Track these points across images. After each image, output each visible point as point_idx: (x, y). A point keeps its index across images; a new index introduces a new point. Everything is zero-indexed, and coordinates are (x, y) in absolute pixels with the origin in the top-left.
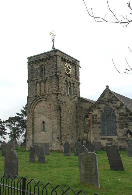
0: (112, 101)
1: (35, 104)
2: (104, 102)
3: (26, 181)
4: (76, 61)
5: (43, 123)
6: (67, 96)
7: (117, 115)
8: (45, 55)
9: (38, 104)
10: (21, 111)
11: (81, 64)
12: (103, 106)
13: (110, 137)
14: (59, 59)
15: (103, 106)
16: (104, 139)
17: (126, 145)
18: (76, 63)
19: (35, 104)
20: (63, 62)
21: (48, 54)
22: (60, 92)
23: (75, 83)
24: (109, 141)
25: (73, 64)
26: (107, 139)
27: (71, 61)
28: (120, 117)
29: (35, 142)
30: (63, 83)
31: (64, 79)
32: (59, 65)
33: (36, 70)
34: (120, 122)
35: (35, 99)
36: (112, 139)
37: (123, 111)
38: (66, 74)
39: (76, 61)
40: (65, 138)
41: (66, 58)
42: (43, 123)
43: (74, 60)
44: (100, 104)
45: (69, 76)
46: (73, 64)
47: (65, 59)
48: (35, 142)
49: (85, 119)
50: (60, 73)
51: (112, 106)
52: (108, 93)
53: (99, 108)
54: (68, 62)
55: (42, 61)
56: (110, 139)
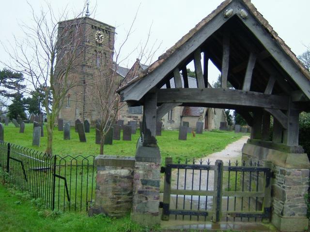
3: (54, 43)
4: (111, 28)
11: (116, 31)
13: (136, 115)
14: (88, 27)
16: (130, 117)
20: (94, 30)
23: (107, 53)
24: (134, 119)
25: (106, 31)
26: (133, 117)
27: (104, 28)
29: (108, 203)
32: (87, 34)
36: (137, 117)
38: (96, 42)
39: (111, 28)
40: (88, 115)
41: (98, 25)
43: (108, 27)
45: (100, 45)
46: (106, 31)
47: (96, 27)
48: (108, 203)
50: (89, 42)
54: (99, 29)
56: (136, 117)
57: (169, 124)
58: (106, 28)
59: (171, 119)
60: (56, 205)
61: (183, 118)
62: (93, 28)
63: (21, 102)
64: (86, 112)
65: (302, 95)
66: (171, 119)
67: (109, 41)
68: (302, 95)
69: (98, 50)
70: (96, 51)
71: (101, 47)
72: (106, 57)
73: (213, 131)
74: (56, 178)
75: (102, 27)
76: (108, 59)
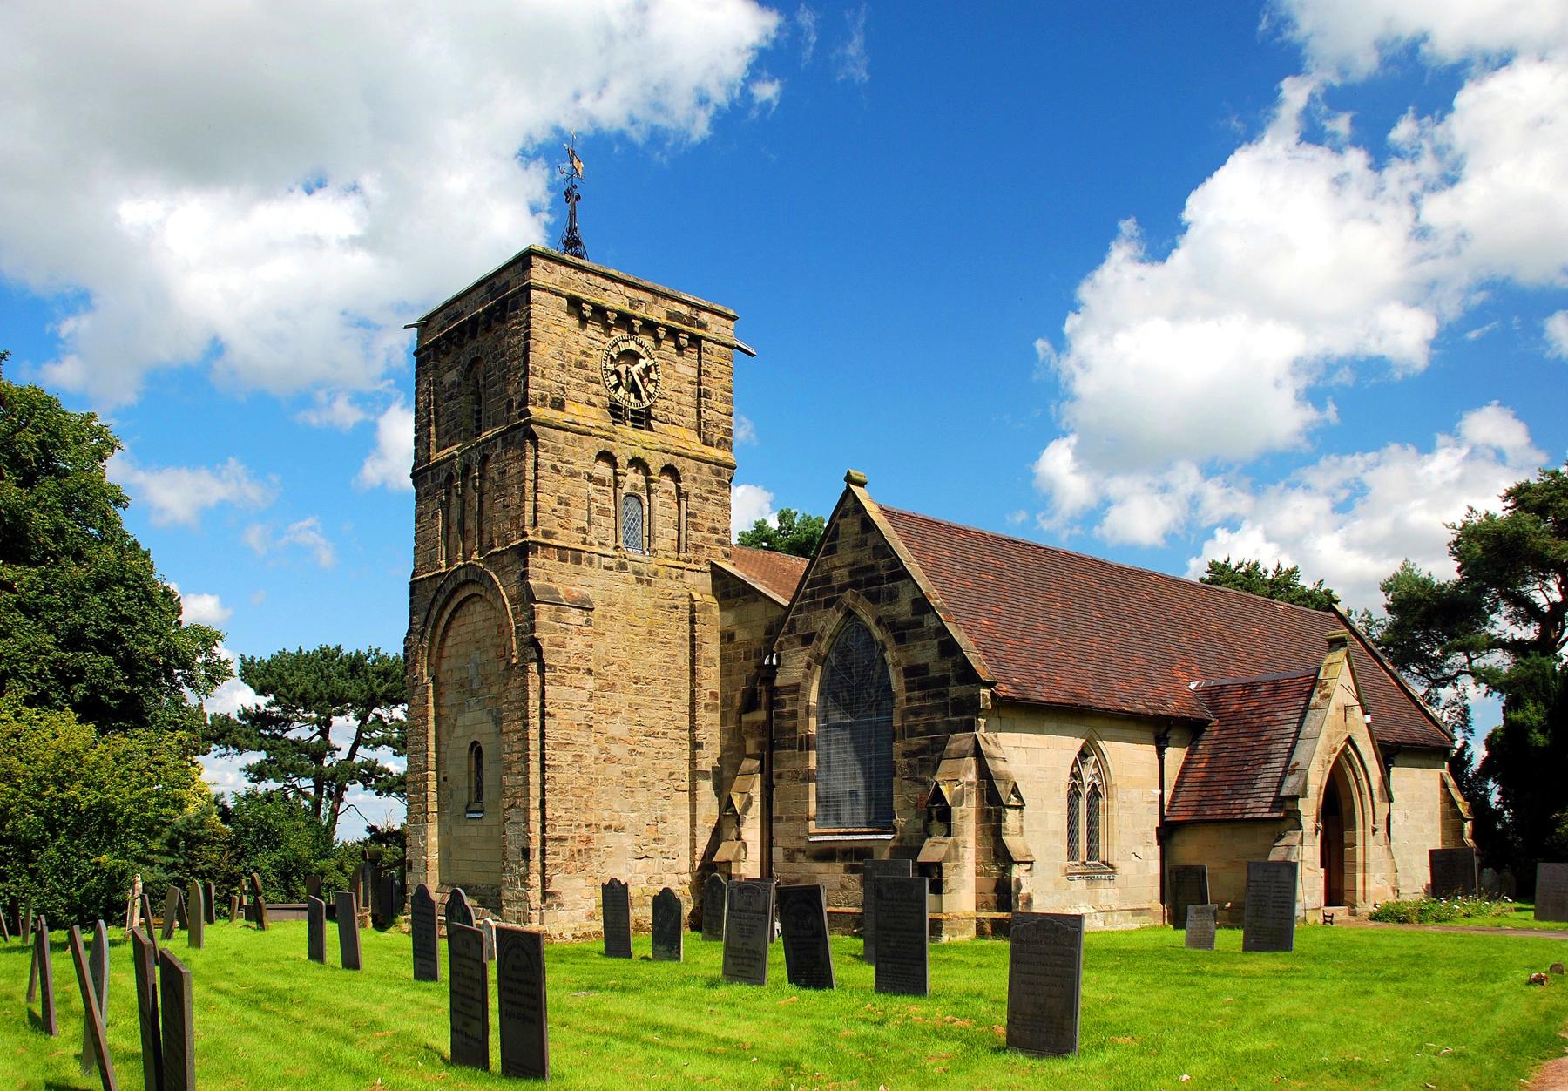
0: (870, 582)
1: (443, 622)
2: (832, 589)
5: (476, 749)
6: (612, 563)
7: (897, 683)
8: (483, 289)
9: (455, 624)
10: (308, 652)
12: (828, 622)
15: (828, 622)
17: (1527, 1078)
18: (703, 326)
19: (443, 622)
21: (498, 283)
22: (547, 534)
28: (909, 700)
30: (573, 474)
31: (592, 446)
33: (450, 398)
34: (912, 732)
35: (438, 591)
37: (927, 653)
42: (476, 749)
44: (815, 605)
49: (745, 718)
50: (559, 405)
51: (869, 621)
52: (850, 527)
53: (807, 639)
55: (474, 336)
57: (1080, 884)
58: (670, 316)
59: (1092, 852)
60: (683, 546)
61: (1177, 839)
62: (583, 321)
63: (1414, 652)
64: (560, 839)
65: (1512, 715)
66: (1092, 852)
67: (701, 394)
68: (1512, 715)
69: (623, 456)
70: (606, 456)
71: (642, 435)
72: (681, 495)
73: (1386, 915)
74: (480, 998)
75: (641, 312)
76: (693, 502)
